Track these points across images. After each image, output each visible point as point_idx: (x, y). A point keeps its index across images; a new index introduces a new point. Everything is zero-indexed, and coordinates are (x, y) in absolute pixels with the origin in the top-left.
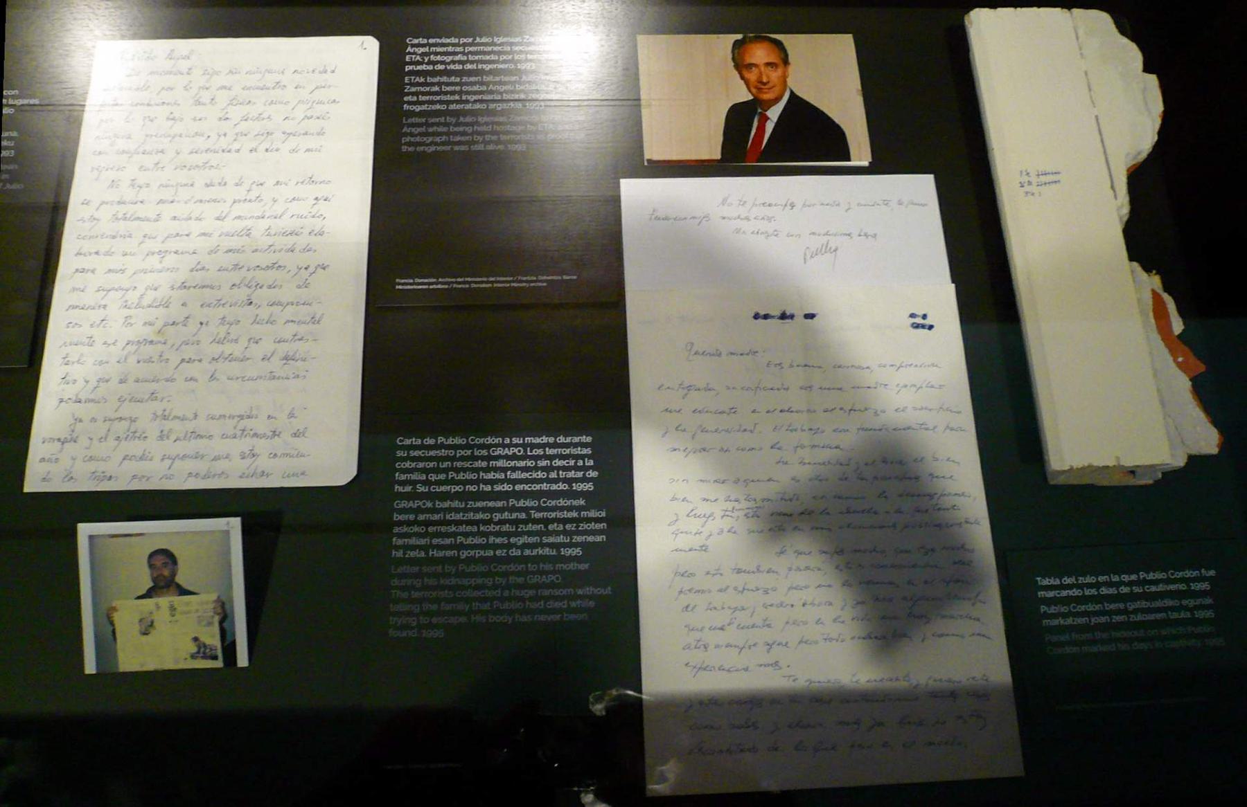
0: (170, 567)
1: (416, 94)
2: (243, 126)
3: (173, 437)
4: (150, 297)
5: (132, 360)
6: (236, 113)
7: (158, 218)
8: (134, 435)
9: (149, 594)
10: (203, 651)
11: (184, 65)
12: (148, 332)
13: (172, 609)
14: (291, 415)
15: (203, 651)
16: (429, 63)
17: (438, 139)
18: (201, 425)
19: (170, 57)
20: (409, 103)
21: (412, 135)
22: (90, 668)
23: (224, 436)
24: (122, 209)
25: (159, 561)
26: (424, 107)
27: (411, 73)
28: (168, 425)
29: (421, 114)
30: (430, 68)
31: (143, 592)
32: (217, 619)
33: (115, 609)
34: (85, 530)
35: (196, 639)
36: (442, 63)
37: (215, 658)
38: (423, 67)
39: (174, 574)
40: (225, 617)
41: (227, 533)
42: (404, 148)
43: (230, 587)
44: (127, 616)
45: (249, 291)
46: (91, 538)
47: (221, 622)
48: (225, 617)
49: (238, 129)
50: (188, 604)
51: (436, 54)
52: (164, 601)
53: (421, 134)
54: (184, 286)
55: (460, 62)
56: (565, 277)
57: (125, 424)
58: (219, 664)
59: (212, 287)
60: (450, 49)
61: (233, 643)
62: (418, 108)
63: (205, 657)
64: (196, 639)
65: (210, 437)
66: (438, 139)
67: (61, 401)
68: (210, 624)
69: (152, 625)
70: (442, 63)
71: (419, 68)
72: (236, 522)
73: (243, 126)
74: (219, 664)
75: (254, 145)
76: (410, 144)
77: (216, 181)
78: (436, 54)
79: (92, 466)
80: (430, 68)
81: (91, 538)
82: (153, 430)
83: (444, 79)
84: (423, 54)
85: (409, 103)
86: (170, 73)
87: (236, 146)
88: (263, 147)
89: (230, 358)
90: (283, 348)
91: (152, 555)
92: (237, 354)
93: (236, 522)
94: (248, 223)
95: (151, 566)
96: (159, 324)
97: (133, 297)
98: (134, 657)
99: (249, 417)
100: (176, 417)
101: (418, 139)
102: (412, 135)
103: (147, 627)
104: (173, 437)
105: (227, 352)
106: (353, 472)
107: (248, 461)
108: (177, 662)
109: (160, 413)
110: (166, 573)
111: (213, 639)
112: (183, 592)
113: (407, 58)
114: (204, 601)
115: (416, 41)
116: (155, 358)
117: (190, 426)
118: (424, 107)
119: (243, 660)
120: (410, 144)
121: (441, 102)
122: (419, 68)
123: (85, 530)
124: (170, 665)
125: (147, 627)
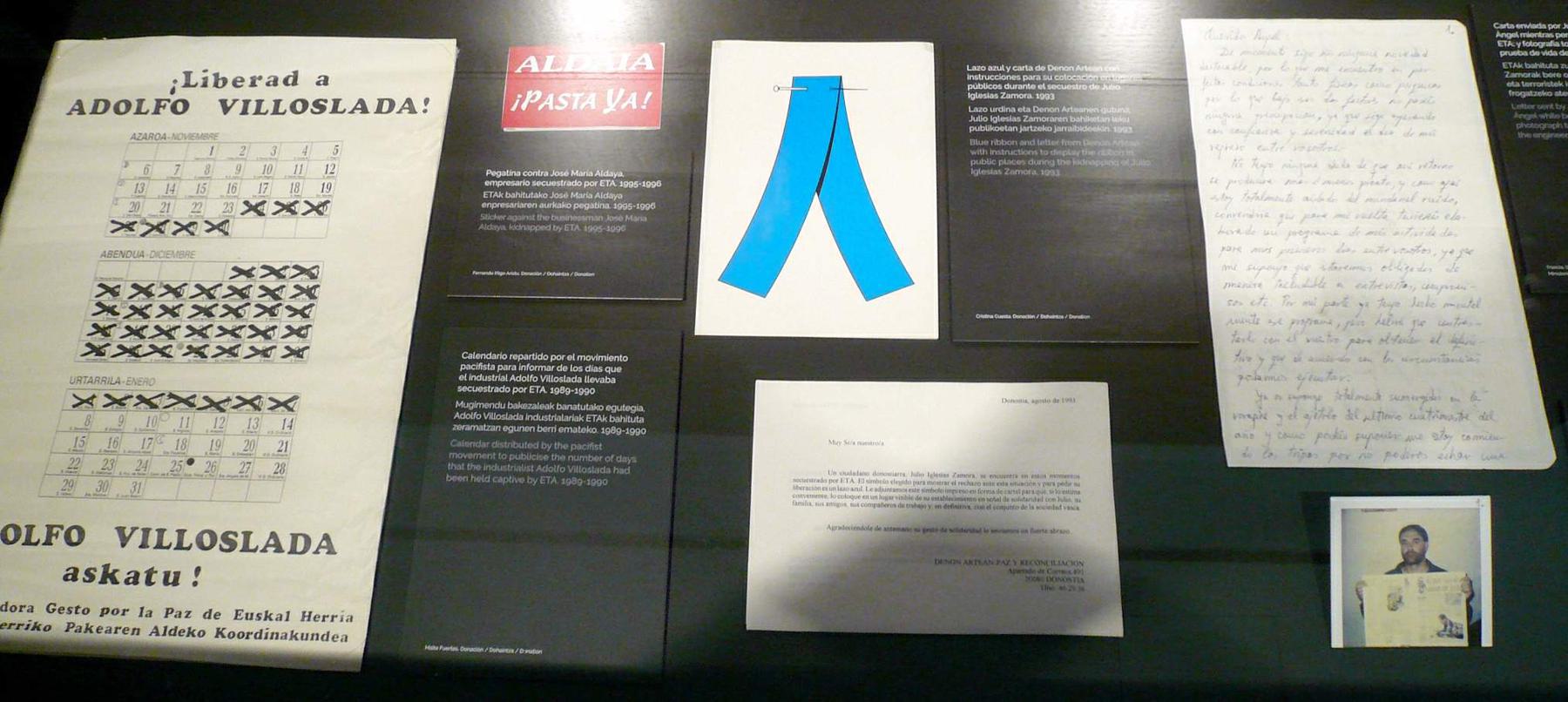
0: (1421, 542)
1: (1519, 80)
2: (1350, 108)
3: (1361, 416)
4: (1302, 277)
5: (1301, 339)
6: (1341, 94)
7: (1290, 198)
8: (1321, 414)
9: (1398, 570)
10: (1449, 629)
11: (1274, 45)
12: (1309, 312)
13: (1422, 585)
14: (1474, 398)
15: (1449, 629)
16: (1523, 48)
17: (1552, 126)
18: (1385, 404)
19: (1258, 36)
20: (1514, 89)
21: (1524, 121)
22: (1337, 641)
23: (1413, 417)
24: (1253, 188)
25: (1412, 534)
26: (1530, 94)
27: (1507, 58)
28: (1354, 404)
29: (1529, 100)
30: (1525, 53)
31: (1394, 567)
32: (1464, 597)
33: (1363, 583)
34: (1337, 504)
35: (1443, 617)
36: (1537, 49)
37: (1461, 637)
38: (1518, 53)
39: (1424, 551)
40: (1472, 596)
41: (1478, 510)
42: (1521, 135)
43: (1478, 565)
44: (1377, 589)
45: (1400, 274)
46: (1343, 511)
47: (1468, 601)
48: (1472, 596)
49: (1347, 111)
50: (1435, 581)
51: (1528, 40)
52: (1414, 577)
53: (1533, 121)
54: (1334, 267)
55: (1554, 49)
56: (1015, 316)
57: (1311, 402)
58: (1464, 643)
59: (1362, 269)
60: (1540, 35)
61: (1479, 622)
62: (1524, 95)
63: (1451, 635)
64: (1443, 617)
65: (1398, 417)
66: (1552, 126)
67: (1241, 378)
68: (1458, 601)
69: (1400, 601)
70: (1537, 49)
71: (1513, 53)
72: (1486, 500)
73: (1350, 108)
74: (1464, 643)
75: (1367, 128)
76: (1524, 130)
77: (1339, 163)
78: (1528, 40)
79: (1289, 443)
80: (1525, 53)
81: (1343, 511)
82: (1340, 408)
83: (1542, 66)
84: (1513, 40)
85: (1514, 89)
86: (1262, 53)
87: (1348, 128)
88: (1377, 129)
89: (1398, 340)
90: (1449, 332)
91: (1404, 530)
92: (1404, 335)
93: (1486, 500)
94: (1384, 205)
95: (1403, 542)
96: (1320, 304)
97: (1286, 276)
98: (1381, 632)
99: (1433, 399)
100: (1359, 397)
101: (1532, 126)
102: (1524, 121)
103: (1395, 604)
104: (1361, 416)
105: (1394, 335)
106: (1553, 458)
107: (1443, 443)
108: (1423, 638)
109: (1342, 392)
110: (1416, 548)
111: (1460, 619)
112: (1433, 568)
113: (969, 77)
114: (1452, 580)
115: (1503, 26)
116: (1325, 338)
117: (1376, 406)
118: (1530, 94)
119: (1487, 640)
120: (1524, 130)
121: (1546, 89)
122: (1513, 53)
123: (1337, 504)
124: (1416, 642)
125: (1395, 604)
